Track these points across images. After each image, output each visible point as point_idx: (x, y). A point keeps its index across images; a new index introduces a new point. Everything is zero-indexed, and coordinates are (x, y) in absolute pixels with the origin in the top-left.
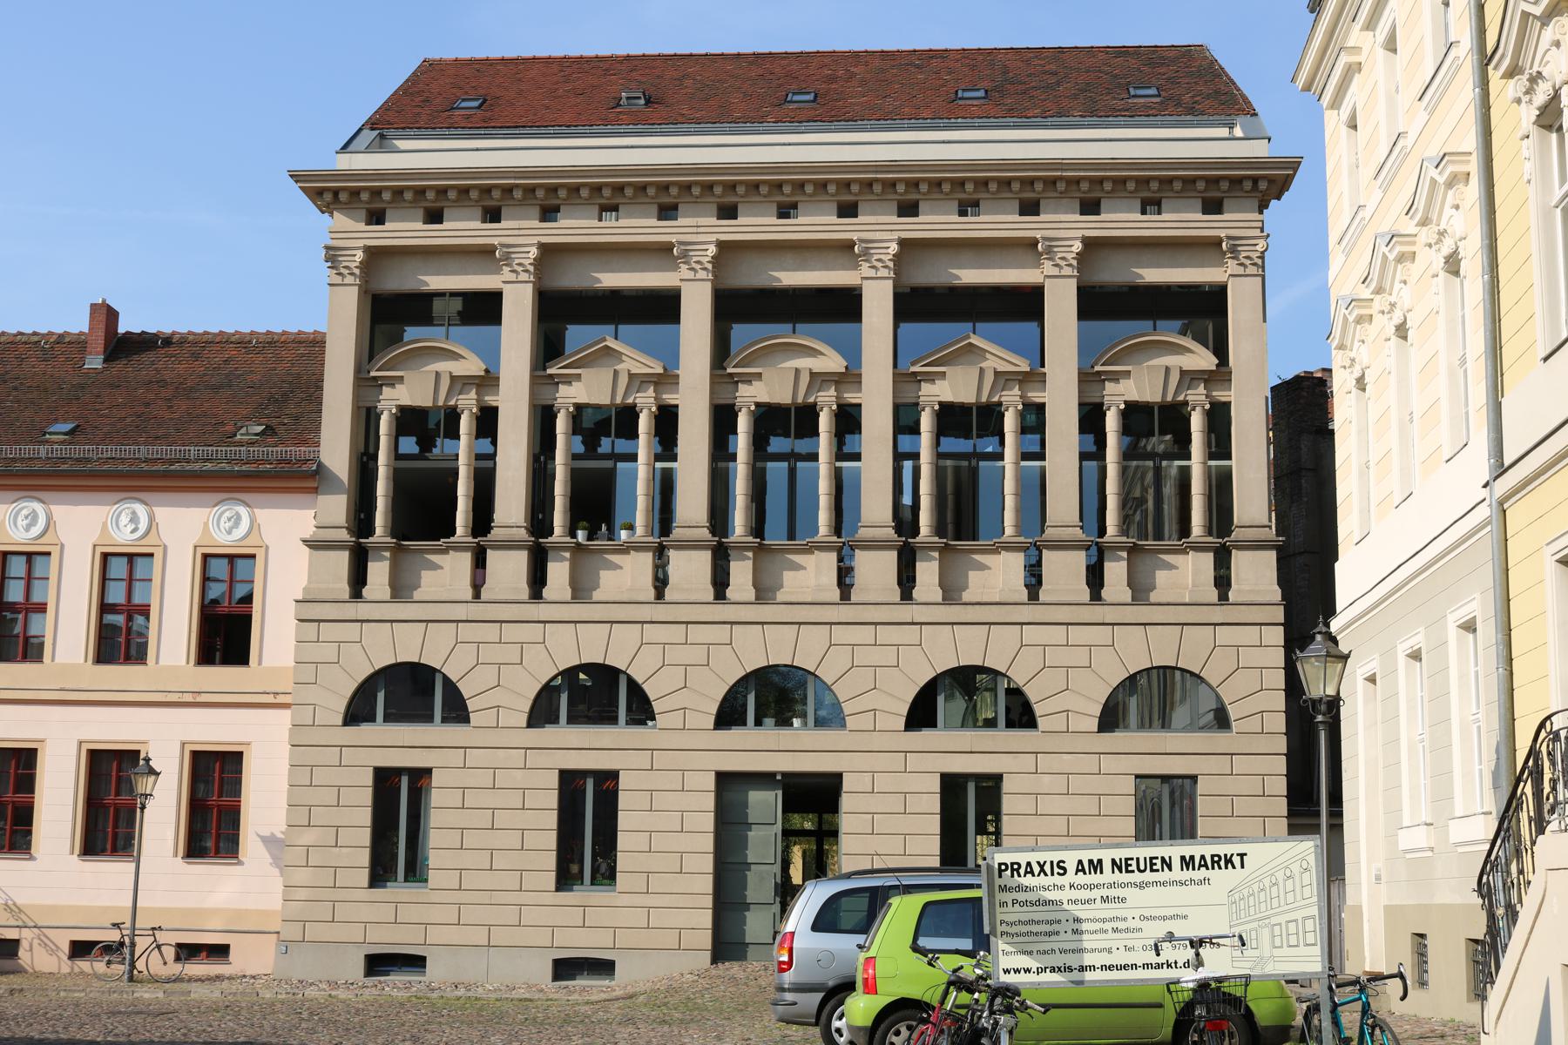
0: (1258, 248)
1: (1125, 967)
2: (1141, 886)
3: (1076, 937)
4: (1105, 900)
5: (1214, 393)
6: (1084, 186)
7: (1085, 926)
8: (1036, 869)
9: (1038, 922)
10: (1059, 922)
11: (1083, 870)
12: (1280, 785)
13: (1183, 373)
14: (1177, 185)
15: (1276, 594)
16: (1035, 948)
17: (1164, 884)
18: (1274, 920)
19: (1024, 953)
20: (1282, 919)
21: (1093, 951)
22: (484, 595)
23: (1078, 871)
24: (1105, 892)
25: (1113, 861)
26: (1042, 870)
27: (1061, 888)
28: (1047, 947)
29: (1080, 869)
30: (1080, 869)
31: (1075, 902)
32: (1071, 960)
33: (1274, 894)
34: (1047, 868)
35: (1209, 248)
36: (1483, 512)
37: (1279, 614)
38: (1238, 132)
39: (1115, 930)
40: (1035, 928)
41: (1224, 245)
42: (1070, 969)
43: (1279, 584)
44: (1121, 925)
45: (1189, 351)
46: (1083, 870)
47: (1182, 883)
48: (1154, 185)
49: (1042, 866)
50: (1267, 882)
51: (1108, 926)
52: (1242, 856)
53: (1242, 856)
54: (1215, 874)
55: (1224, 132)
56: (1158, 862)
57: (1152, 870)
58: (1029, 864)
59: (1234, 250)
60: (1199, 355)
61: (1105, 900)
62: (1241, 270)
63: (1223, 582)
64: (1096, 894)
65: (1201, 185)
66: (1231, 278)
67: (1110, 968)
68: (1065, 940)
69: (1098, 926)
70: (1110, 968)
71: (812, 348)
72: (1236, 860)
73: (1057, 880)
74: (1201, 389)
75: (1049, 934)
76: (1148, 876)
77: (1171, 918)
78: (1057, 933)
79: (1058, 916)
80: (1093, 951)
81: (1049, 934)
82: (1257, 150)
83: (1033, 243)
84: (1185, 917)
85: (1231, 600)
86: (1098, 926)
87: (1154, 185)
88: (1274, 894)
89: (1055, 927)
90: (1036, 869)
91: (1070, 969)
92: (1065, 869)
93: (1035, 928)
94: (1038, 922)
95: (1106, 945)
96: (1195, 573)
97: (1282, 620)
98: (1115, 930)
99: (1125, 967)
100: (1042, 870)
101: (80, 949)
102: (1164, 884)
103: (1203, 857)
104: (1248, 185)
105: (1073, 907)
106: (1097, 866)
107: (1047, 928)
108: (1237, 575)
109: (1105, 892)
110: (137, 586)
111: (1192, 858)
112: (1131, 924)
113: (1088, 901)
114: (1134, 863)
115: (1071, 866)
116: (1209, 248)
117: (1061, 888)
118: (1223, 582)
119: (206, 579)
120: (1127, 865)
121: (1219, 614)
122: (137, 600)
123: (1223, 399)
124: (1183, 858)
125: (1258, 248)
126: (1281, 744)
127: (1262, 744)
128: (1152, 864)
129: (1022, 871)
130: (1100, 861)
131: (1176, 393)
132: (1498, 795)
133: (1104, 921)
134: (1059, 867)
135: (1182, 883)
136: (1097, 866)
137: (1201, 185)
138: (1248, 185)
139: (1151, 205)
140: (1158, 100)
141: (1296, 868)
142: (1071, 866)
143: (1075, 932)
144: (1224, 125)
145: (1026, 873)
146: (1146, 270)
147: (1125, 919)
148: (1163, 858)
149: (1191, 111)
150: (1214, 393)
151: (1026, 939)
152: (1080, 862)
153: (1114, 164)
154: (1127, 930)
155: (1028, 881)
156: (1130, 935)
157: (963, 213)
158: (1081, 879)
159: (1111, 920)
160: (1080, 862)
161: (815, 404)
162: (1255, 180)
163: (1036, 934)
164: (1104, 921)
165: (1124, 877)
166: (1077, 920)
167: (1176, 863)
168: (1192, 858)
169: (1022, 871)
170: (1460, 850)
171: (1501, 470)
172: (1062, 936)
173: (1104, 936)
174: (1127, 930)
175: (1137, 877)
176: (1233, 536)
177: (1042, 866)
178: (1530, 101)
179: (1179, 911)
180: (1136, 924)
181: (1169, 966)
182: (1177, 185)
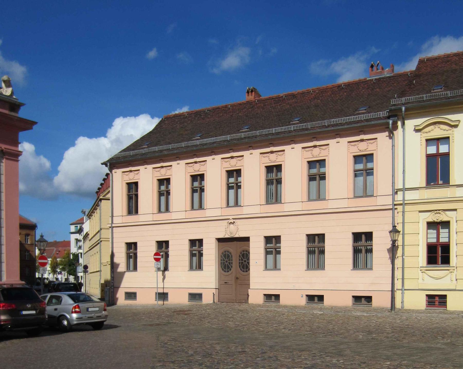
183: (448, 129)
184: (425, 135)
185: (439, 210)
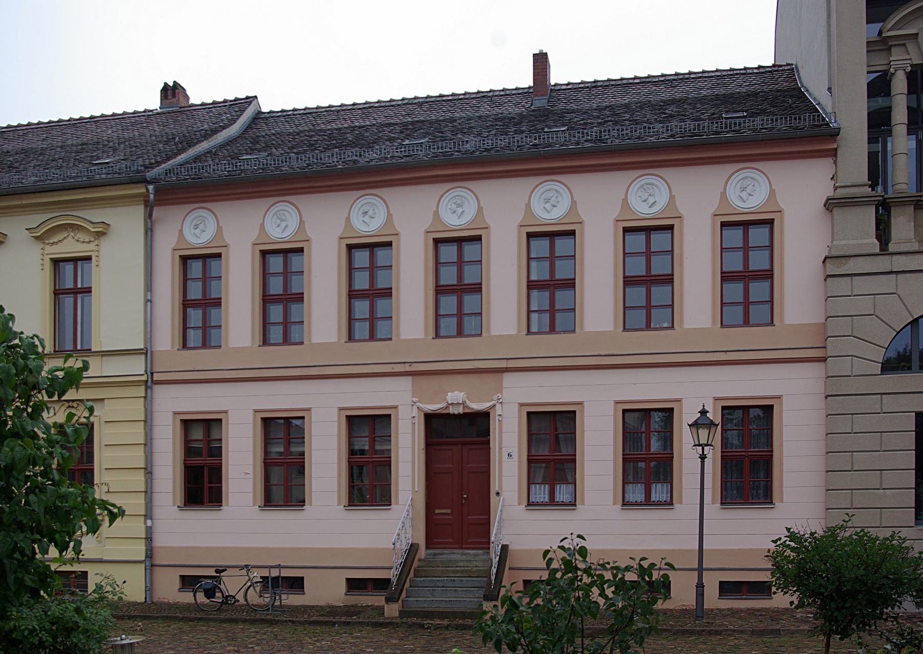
101: (354, 585)
110: (380, 274)
119: (351, 269)
122: (381, 284)
183: (88, 240)
184: (49, 249)
185: (73, 401)
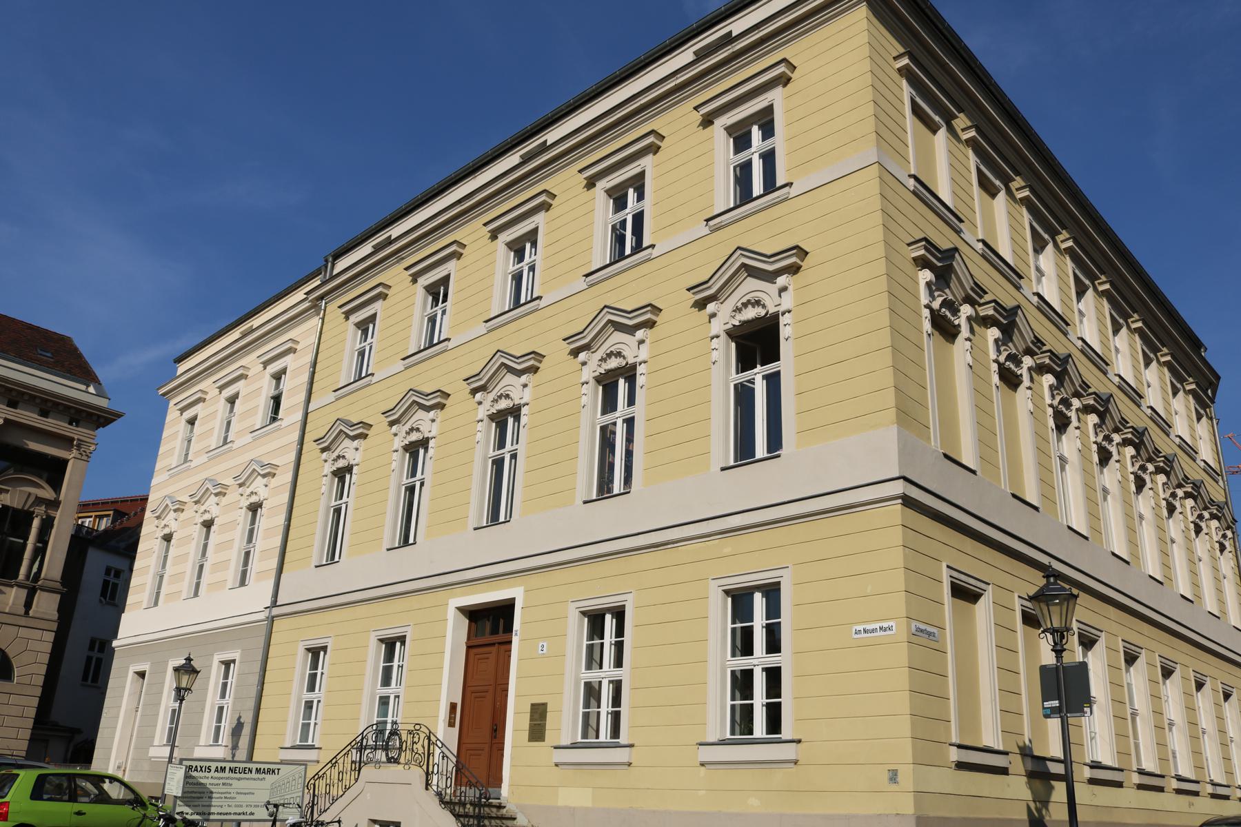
0: (91, 448)
1: (226, 814)
2: (239, 779)
3: (210, 800)
4: (224, 784)
5: (49, 511)
6: (14, 394)
7: (214, 795)
8: (199, 769)
9: (196, 793)
10: (204, 793)
11: (218, 771)
12: (32, 713)
13: (37, 498)
14: (61, 408)
15: (55, 616)
16: (192, 804)
17: (248, 779)
18: (286, 797)
19: (187, 806)
20: (288, 797)
21: (215, 806)
22: (31, 613)
23: (215, 771)
24: (224, 781)
25: (230, 768)
26: (201, 770)
27: (208, 778)
28: (196, 803)
29: (217, 770)
30: (217, 770)
31: (212, 784)
32: (205, 810)
33: (293, 784)
34: (203, 769)
35: (67, 442)
36: (262, 616)
37: (54, 626)
38: (91, 389)
39: (225, 798)
40: (193, 795)
41: (75, 442)
42: (204, 814)
43: (58, 611)
44: (228, 796)
45: (43, 488)
46: (218, 771)
47: (254, 779)
48: (50, 404)
49: (201, 768)
50: (291, 779)
51: (223, 796)
52: (279, 769)
53: (279, 769)
54: (267, 777)
55: (83, 387)
56: (247, 769)
57: (244, 773)
58: (196, 767)
59: (79, 446)
60: (47, 491)
61: (224, 784)
62: (79, 456)
63: (28, 605)
64: (221, 781)
65: (72, 411)
66: (73, 459)
67: (220, 814)
68: (204, 801)
69: (219, 795)
70: (220, 814)
71: (38, 484)
72: (276, 771)
73: (207, 774)
74: (43, 508)
75: (199, 798)
76: (243, 775)
77: (248, 794)
78: (202, 798)
79: (204, 790)
80: (215, 806)
81: (199, 798)
82: (102, 403)
83: (72, 440)
84: (253, 794)
85: (31, 615)
86: (219, 795)
87: (50, 404)
88: (293, 784)
89: (202, 795)
90: (199, 769)
91: (204, 814)
92: (210, 770)
93: (193, 795)
94: (196, 793)
95: (221, 804)
96: (16, 597)
97: (55, 629)
98: (225, 798)
99: (226, 814)
100: (201, 770)
102: (248, 779)
103: (264, 769)
104: (95, 418)
105: (211, 787)
106: (223, 769)
107: (199, 795)
108: (38, 603)
109: (224, 781)
111: (260, 769)
112: (232, 795)
113: (217, 785)
114: (238, 769)
115: (213, 769)
116: (67, 442)
117: (208, 778)
118: (28, 605)
120: (235, 770)
121: (23, 621)
123: (52, 515)
124: (257, 769)
125: (91, 448)
126: (38, 692)
127: (29, 691)
128: (245, 770)
129: (193, 769)
130: (225, 768)
131: (30, 507)
132: (234, 739)
133: (222, 793)
134: (208, 769)
135: (254, 779)
136: (223, 769)
137: (72, 411)
138: (95, 418)
139: (44, 413)
140: (52, 360)
141: (297, 776)
142: (213, 769)
143: (209, 797)
144: (85, 384)
145: (195, 770)
146: (32, 443)
147: (230, 793)
148: (249, 769)
149: (69, 372)
150: (49, 511)
151: (189, 800)
152: (217, 767)
153: (34, 389)
154: (230, 798)
155: (201, 774)
156: (230, 800)
157: (70, 424)
158: (216, 775)
159: (224, 793)
160: (217, 767)
161: (33, 512)
162: (99, 416)
163: (194, 798)
164: (222, 793)
165: (233, 775)
166: (212, 792)
167: (254, 771)
168: (260, 769)
169: (193, 769)
170: (153, 759)
171: (274, 604)
172: (204, 799)
173: (220, 800)
174: (230, 798)
175: (238, 775)
176: (40, 583)
177: (201, 768)
178: (333, 464)
179: (250, 791)
180: (235, 795)
181: (244, 814)
182: (61, 408)
